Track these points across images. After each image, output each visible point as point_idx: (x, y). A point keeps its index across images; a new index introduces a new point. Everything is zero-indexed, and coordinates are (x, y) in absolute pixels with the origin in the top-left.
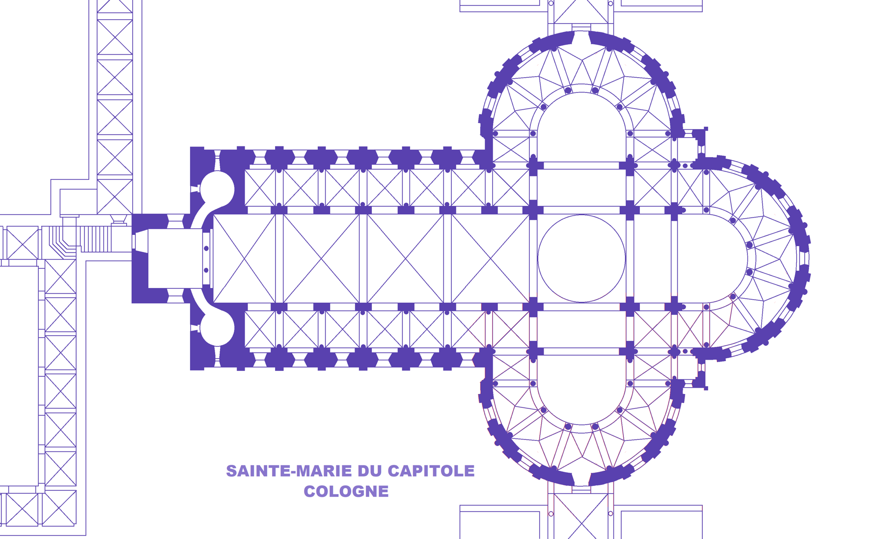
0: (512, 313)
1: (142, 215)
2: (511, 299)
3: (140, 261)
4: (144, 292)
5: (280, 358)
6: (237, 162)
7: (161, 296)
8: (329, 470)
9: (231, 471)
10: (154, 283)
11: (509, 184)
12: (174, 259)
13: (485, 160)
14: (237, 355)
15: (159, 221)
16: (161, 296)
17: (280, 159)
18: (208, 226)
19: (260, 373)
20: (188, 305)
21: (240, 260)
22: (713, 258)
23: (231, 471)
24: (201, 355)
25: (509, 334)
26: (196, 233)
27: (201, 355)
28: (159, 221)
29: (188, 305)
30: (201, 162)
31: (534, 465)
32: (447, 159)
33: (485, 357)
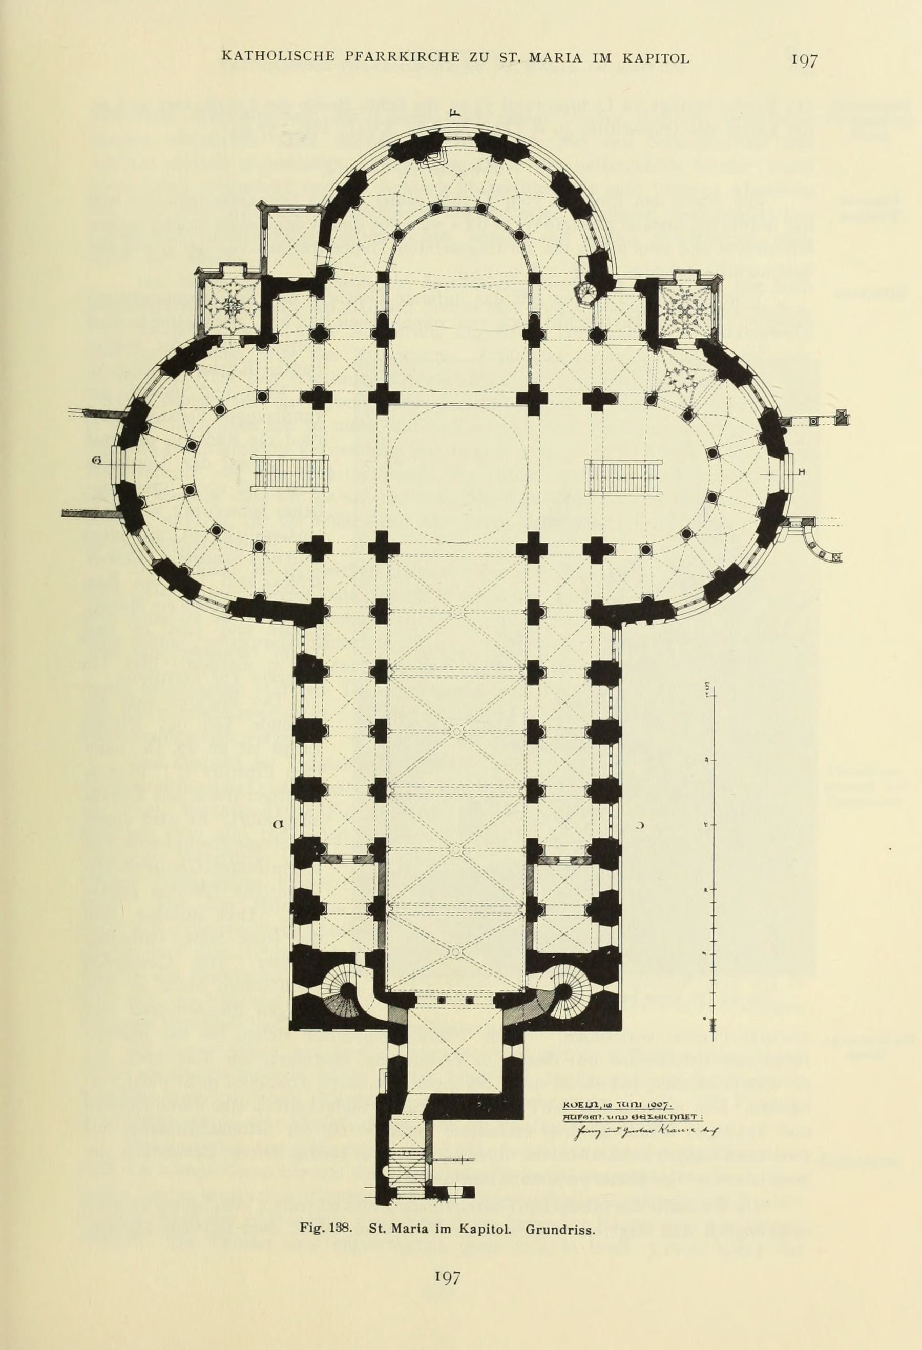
1: (314, 742)
4: (507, 1103)
5: (605, 909)
6: (309, 964)
7: (513, 1071)
10: (494, 1085)
11: (346, 581)
12: (456, 1050)
13: (311, 614)
14: (603, 964)
16: (513, 1071)
17: (306, 907)
18: (407, 1001)
19: (627, 936)
21: (456, 956)
24: (604, 1015)
26: (415, 1019)
27: (604, 1015)
29: (528, 1035)
31: (617, 892)
32: (309, 670)
33: (603, 614)
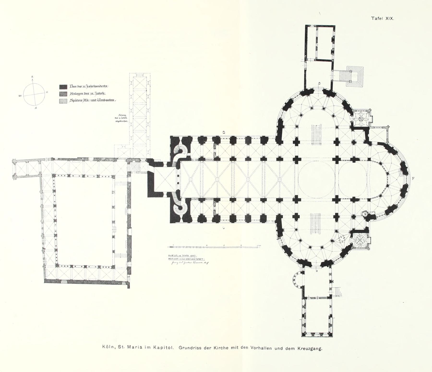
0: (288, 201)
2: (335, 208)
3: (151, 176)
5: (202, 219)
6: (187, 141)
7: (160, 195)
8: (94, 100)
9: (113, 100)
11: (288, 150)
12: (165, 180)
13: (279, 140)
14: (187, 218)
15: (160, 164)
16: (160, 195)
17: (202, 140)
18: (178, 166)
20: (169, 198)
22: (371, 180)
23: (113, 100)
24: (174, 218)
25: (287, 209)
26: (173, 169)
27: (174, 218)
28: (160, 164)
30: (174, 141)
32: (264, 140)
